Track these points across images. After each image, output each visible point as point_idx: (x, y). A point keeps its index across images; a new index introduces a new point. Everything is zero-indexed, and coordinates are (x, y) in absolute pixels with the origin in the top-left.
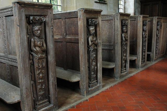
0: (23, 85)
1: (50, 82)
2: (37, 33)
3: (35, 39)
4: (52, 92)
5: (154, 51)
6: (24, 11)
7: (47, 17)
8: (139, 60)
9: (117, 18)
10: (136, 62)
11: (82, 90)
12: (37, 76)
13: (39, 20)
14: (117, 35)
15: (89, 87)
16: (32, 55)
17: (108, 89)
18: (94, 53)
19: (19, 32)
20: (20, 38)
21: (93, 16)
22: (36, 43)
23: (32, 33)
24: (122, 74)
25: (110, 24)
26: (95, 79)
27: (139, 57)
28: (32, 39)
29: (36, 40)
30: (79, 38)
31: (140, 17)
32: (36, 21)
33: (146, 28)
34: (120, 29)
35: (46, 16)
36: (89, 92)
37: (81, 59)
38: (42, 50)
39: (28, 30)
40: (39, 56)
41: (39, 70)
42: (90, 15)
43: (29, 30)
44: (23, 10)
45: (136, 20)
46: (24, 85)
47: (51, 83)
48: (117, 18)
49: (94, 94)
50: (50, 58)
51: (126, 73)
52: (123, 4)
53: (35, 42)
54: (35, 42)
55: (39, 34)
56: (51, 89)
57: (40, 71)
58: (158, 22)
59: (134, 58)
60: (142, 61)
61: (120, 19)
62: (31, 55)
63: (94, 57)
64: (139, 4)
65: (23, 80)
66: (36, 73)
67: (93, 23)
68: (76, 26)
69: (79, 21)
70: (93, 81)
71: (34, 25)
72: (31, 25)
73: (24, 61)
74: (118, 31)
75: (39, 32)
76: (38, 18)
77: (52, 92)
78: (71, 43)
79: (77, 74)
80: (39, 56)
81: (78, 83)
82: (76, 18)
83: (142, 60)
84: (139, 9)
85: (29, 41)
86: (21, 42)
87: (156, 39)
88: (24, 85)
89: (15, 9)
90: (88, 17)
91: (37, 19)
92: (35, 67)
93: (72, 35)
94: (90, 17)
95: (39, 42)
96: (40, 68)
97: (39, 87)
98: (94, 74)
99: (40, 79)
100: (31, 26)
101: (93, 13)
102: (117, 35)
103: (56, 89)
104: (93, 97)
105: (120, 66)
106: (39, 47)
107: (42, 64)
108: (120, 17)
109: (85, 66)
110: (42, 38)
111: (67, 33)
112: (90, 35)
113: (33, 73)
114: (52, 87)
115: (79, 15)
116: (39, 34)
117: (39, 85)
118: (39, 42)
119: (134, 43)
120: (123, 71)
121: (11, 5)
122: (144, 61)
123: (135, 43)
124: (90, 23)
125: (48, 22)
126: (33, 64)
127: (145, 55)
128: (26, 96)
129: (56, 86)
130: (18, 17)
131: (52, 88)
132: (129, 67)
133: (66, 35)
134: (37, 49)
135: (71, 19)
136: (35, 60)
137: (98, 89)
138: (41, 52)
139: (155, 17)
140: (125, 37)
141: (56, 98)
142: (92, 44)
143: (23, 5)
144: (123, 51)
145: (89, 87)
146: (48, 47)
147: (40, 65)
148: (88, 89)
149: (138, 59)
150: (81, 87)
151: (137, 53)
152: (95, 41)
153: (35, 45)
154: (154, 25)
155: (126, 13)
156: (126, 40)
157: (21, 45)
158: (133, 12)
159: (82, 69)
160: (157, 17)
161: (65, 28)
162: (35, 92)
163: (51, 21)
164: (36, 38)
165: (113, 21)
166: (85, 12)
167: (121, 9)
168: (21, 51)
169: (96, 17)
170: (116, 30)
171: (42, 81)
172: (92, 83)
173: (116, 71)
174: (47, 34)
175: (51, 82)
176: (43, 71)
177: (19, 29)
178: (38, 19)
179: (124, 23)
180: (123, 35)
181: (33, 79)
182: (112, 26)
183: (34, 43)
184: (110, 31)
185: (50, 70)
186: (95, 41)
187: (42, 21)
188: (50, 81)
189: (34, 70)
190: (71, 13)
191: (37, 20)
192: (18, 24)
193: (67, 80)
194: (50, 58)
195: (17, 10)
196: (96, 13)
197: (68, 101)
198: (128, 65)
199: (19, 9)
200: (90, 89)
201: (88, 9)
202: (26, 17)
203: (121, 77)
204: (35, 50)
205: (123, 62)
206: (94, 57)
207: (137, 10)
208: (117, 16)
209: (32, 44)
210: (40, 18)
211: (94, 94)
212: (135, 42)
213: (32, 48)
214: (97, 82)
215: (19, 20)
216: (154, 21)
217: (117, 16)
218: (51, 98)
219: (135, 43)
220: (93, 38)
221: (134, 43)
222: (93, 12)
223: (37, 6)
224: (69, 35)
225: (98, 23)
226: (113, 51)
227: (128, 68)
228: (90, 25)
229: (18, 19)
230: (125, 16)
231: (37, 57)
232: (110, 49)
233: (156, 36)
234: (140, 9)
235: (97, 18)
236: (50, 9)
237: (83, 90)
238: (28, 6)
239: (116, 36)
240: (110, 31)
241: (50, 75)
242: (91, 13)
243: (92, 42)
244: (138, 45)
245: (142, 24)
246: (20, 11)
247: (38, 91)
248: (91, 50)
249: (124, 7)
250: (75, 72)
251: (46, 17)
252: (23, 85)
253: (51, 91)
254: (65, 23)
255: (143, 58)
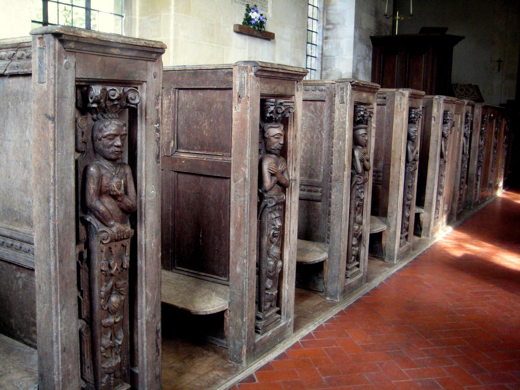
0: (54, 339)
1: (139, 321)
2: (112, 145)
3: (102, 166)
4: (145, 356)
5: (431, 203)
6: (73, 65)
7: (142, 88)
8: (395, 232)
9: (342, 97)
10: (383, 242)
11: (231, 342)
12: (98, 302)
13: (118, 99)
14: (339, 151)
15: (257, 330)
16: (87, 224)
17: (310, 334)
18: (278, 215)
19: (51, 144)
20: (52, 164)
21: (280, 89)
22: (105, 182)
23: (90, 145)
24: (349, 281)
25: (313, 113)
26: (274, 303)
27: (393, 223)
28: (92, 169)
29: (103, 171)
30: (232, 162)
31: (403, 95)
32: (109, 104)
33: (417, 130)
34: (348, 135)
35: (141, 83)
36: (254, 350)
37: (238, 236)
38: (122, 210)
39: (80, 134)
40: (114, 229)
41: (107, 281)
42: (273, 86)
43: (83, 133)
44: (69, 60)
45: (388, 103)
46: (57, 337)
47: (142, 324)
48: (342, 97)
49: (271, 357)
50: (146, 237)
51: (358, 277)
52: (319, 43)
53: (100, 177)
54: (100, 177)
55: (117, 149)
56: (143, 345)
57: (111, 283)
58: (445, 113)
59: (380, 227)
60: (401, 238)
61: (351, 100)
62: (82, 227)
63: (276, 229)
64: (368, 46)
65: (54, 318)
66: (96, 291)
67: (279, 113)
68: (217, 120)
69: (235, 103)
70: (268, 310)
71: (100, 116)
72: (89, 115)
73: (63, 250)
74: (344, 140)
75: (119, 143)
76: (116, 92)
77: (145, 356)
78: (193, 177)
79: (213, 285)
80: (114, 229)
81: (220, 316)
82: (218, 92)
83: (401, 233)
84: (367, 62)
85: (80, 176)
86: (54, 181)
87: (440, 165)
88: (57, 337)
89: (41, 59)
90: (265, 92)
91: (114, 96)
92: (96, 272)
93: (200, 150)
94: (272, 92)
95: (116, 180)
96: (112, 275)
97: (105, 341)
98: (272, 287)
99: (110, 312)
100: (91, 121)
101: (282, 79)
102: (339, 151)
103: (157, 346)
104: (268, 366)
105: (344, 254)
106: (115, 197)
107: (120, 257)
108: (352, 94)
109: (250, 261)
110: (122, 164)
111: (182, 140)
112: (269, 152)
113: (86, 293)
114: (145, 339)
115: (236, 83)
116: (117, 149)
117: (106, 333)
118: (116, 180)
119: (379, 176)
120: (350, 273)
121: (30, 38)
122: (406, 237)
123: (381, 178)
124: (272, 112)
125: (144, 108)
126: (89, 262)
127: (409, 217)
128: (61, 378)
129: (160, 335)
130: (52, 87)
131: (145, 344)
132: (367, 258)
133: (178, 145)
134: (107, 205)
135: (200, 93)
136: (95, 244)
137: (280, 336)
138: (120, 214)
139: (437, 97)
140: (362, 161)
141: (158, 377)
142: (274, 184)
143: (72, 45)
144: (353, 206)
145: (257, 330)
146: (141, 196)
147: (114, 264)
148: (254, 338)
149: (392, 230)
150: (230, 330)
151: (389, 210)
152: (283, 173)
153: (101, 191)
154: (433, 122)
155: (74, 25)
156: (365, 169)
157: (55, 190)
158: (351, 71)
159: (238, 270)
160: (444, 97)
161: (175, 123)
162: (88, 361)
163: (156, 104)
164: (106, 164)
165: (325, 105)
166: (259, 73)
167: (313, 59)
168: (54, 213)
169: (289, 93)
170: (336, 135)
171: (117, 320)
172: (266, 318)
173: (328, 272)
174: (139, 150)
175: (144, 322)
176: (120, 283)
177: (51, 131)
178: (117, 95)
179: (362, 113)
180: (357, 153)
181: (85, 313)
182: (322, 121)
183: (98, 182)
184: (312, 137)
185: (144, 279)
186: (283, 173)
187: (128, 101)
188: (139, 317)
189: (91, 281)
190: (201, 74)
191: (115, 100)
192: (51, 113)
193: (181, 306)
194: (146, 237)
195: (48, 58)
196: (289, 79)
197: (188, 382)
198: (365, 252)
199: (58, 58)
200: (259, 338)
201: (269, 66)
202: (78, 87)
203: (344, 291)
204: (102, 208)
205: (354, 243)
206: (276, 229)
207: (361, 67)
208: (342, 89)
209: (92, 187)
210: (123, 90)
211: (271, 357)
212: (381, 174)
213: (89, 200)
214: (279, 312)
215: (55, 97)
216: (435, 110)
217: (342, 89)
218: (140, 380)
219: (381, 178)
220: (277, 164)
221: (379, 176)
222: (281, 75)
223: (115, 48)
224: (189, 148)
225: (294, 115)
226: (319, 203)
227: (364, 263)
228: (270, 120)
229: (51, 96)
230: (364, 91)
231: (104, 234)
232: (312, 196)
233: (438, 157)
234: (369, 64)
235: (291, 96)
236: (154, 60)
237: (237, 342)
238: (88, 49)
239: (336, 155)
240: (312, 137)
241: (142, 298)
242: (275, 78)
243: (275, 178)
244: (390, 184)
245: (407, 119)
246: (60, 63)
247: (99, 357)
248: (270, 205)
249: (320, 52)
250: (205, 278)
251: (139, 87)
252: (54, 339)
253: (143, 354)
254: (176, 106)
255: (405, 228)
